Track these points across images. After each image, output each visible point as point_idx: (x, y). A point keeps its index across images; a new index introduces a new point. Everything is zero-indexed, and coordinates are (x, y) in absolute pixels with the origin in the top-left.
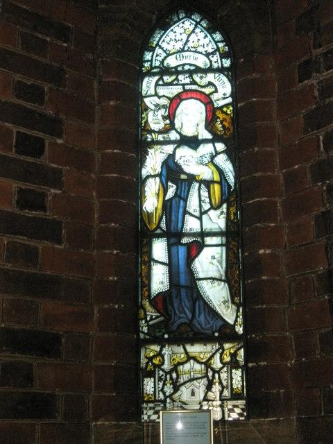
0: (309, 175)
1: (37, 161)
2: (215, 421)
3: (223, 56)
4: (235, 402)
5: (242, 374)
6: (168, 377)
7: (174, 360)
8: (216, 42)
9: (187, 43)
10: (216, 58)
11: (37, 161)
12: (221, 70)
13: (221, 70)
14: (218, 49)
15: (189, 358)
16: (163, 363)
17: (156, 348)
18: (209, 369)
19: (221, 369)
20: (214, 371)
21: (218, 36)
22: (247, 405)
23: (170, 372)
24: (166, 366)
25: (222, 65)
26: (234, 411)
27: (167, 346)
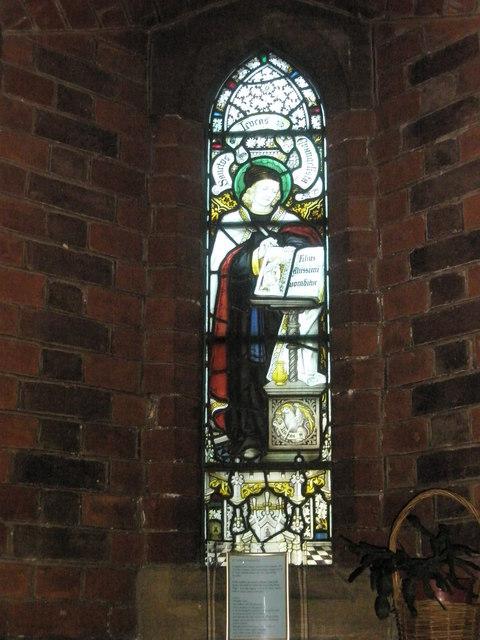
0: (415, 471)
1: (458, 303)
2: (292, 566)
3: (312, 111)
4: (319, 544)
5: (328, 507)
6: (238, 511)
7: (244, 491)
8: (300, 89)
9: (267, 99)
10: (301, 113)
11: (458, 303)
12: (310, 133)
13: (310, 133)
14: (305, 100)
15: (267, 488)
16: (232, 496)
17: (224, 476)
18: (289, 505)
19: (304, 502)
20: (295, 506)
21: (301, 82)
22: (334, 547)
23: (240, 506)
24: (237, 499)
25: (311, 125)
26: (316, 554)
27: (236, 474)
